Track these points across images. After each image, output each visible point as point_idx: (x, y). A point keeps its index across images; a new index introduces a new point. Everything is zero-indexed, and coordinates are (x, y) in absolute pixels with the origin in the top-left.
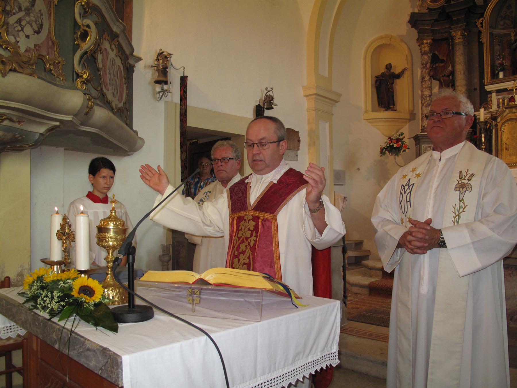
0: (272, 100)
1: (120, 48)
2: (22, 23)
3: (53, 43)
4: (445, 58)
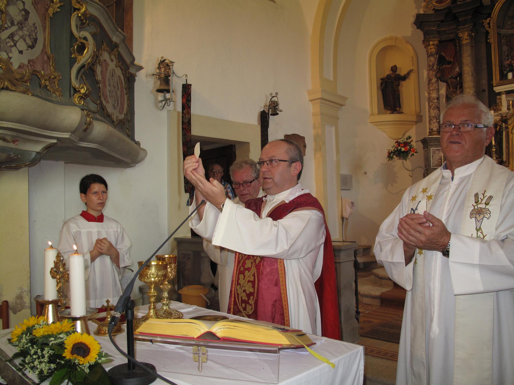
0: (277, 106)
1: (120, 58)
2: (14, 39)
3: (49, 58)
4: (452, 60)
